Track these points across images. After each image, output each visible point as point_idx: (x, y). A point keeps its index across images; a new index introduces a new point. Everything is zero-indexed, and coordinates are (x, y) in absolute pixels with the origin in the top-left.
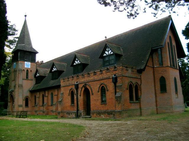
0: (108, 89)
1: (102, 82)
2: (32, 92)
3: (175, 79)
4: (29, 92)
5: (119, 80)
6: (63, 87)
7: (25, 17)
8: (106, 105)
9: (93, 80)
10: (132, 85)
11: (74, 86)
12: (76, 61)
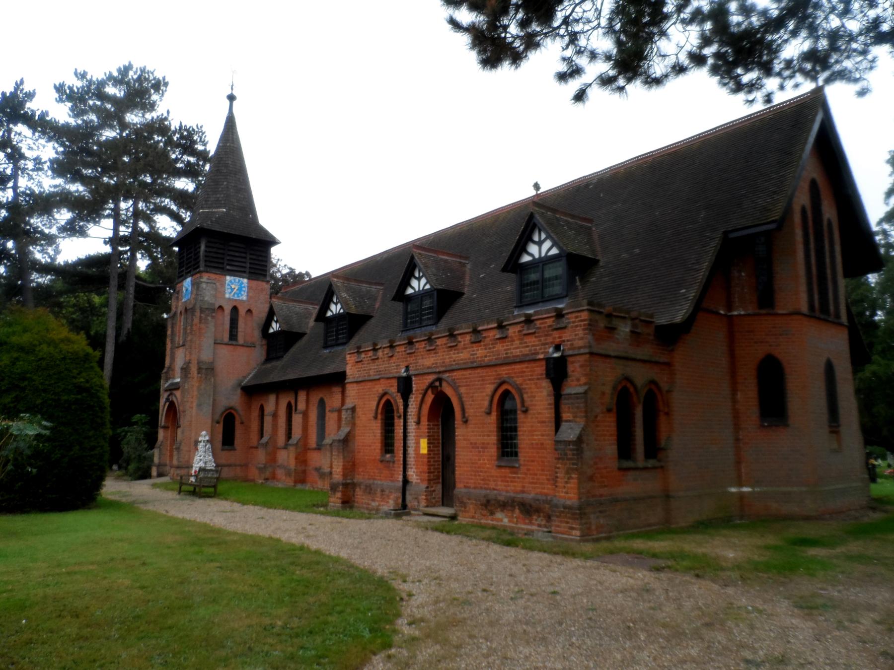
0: (526, 404)
1: (504, 371)
2: (253, 391)
3: (829, 369)
4: (239, 391)
5: (575, 368)
6: (357, 382)
7: (228, 102)
8: (515, 470)
9: (466, 362)
10: (632, 390)
11: (395, 383)
12: (416, 278)
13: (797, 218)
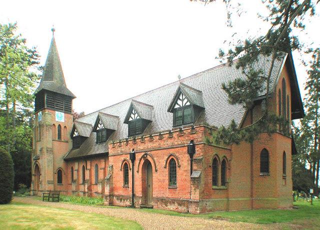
1: (171, 151)
2: (67, 161)
3: (284, 153)
11: (129, 156)
13: (277, 93)
